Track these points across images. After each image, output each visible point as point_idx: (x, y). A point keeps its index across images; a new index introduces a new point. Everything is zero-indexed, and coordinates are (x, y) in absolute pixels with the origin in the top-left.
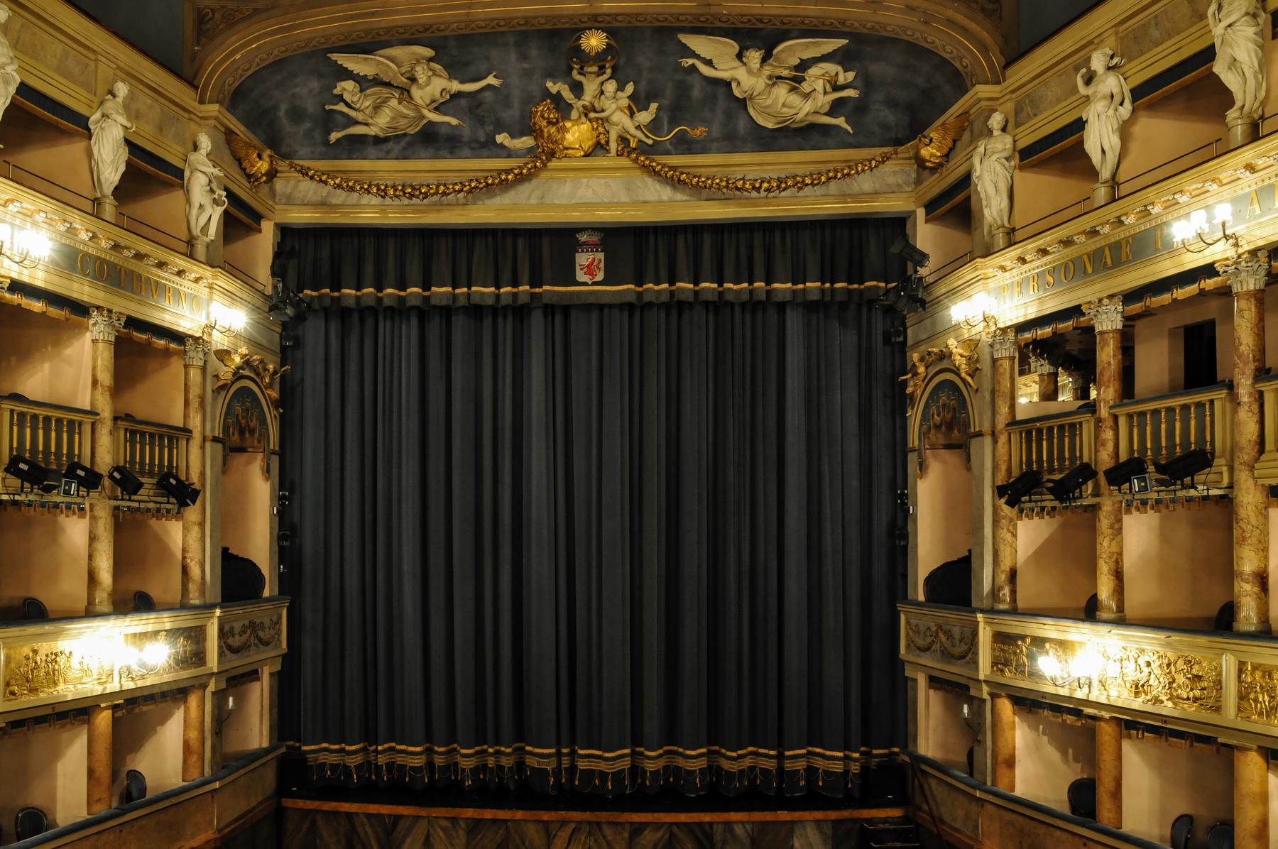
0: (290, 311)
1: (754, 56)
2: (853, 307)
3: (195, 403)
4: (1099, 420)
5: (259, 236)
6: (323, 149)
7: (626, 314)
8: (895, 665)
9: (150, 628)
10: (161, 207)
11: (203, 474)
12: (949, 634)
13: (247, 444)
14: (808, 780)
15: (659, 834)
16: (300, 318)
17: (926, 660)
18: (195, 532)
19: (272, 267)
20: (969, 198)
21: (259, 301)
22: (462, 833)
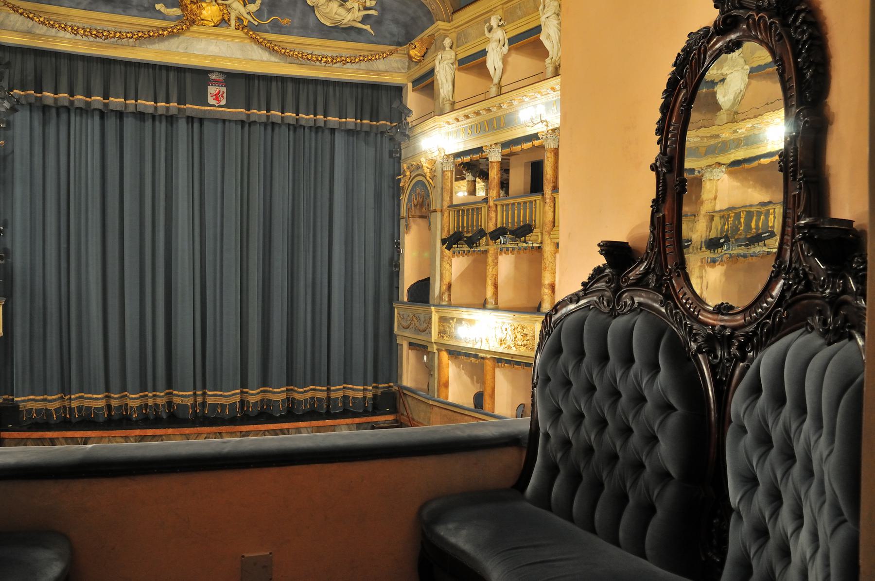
4: (489, 207)
7: (239, 127)
12: (418, 319)
14: (344, 403)
17: (407, 333)
20: (433, 82)
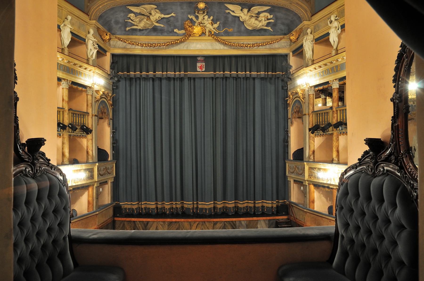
0: (116, 79)
1: (246, 11)
2: (273, 79)
3: (90, 105)
4: (333, 111)
5: (106, 57)
6: (124, 32)
8: (285, 177)
9: (79, 168)
10: (79, 49)
11: (92, 125)
12: (298, 168)
13: (103, 117)
14: (262, 210)
15: (222, 224)
16: (119, 81)
18: (90, 142)
19: (111, 66)
21: (106, 76)
22: (166, 226)
